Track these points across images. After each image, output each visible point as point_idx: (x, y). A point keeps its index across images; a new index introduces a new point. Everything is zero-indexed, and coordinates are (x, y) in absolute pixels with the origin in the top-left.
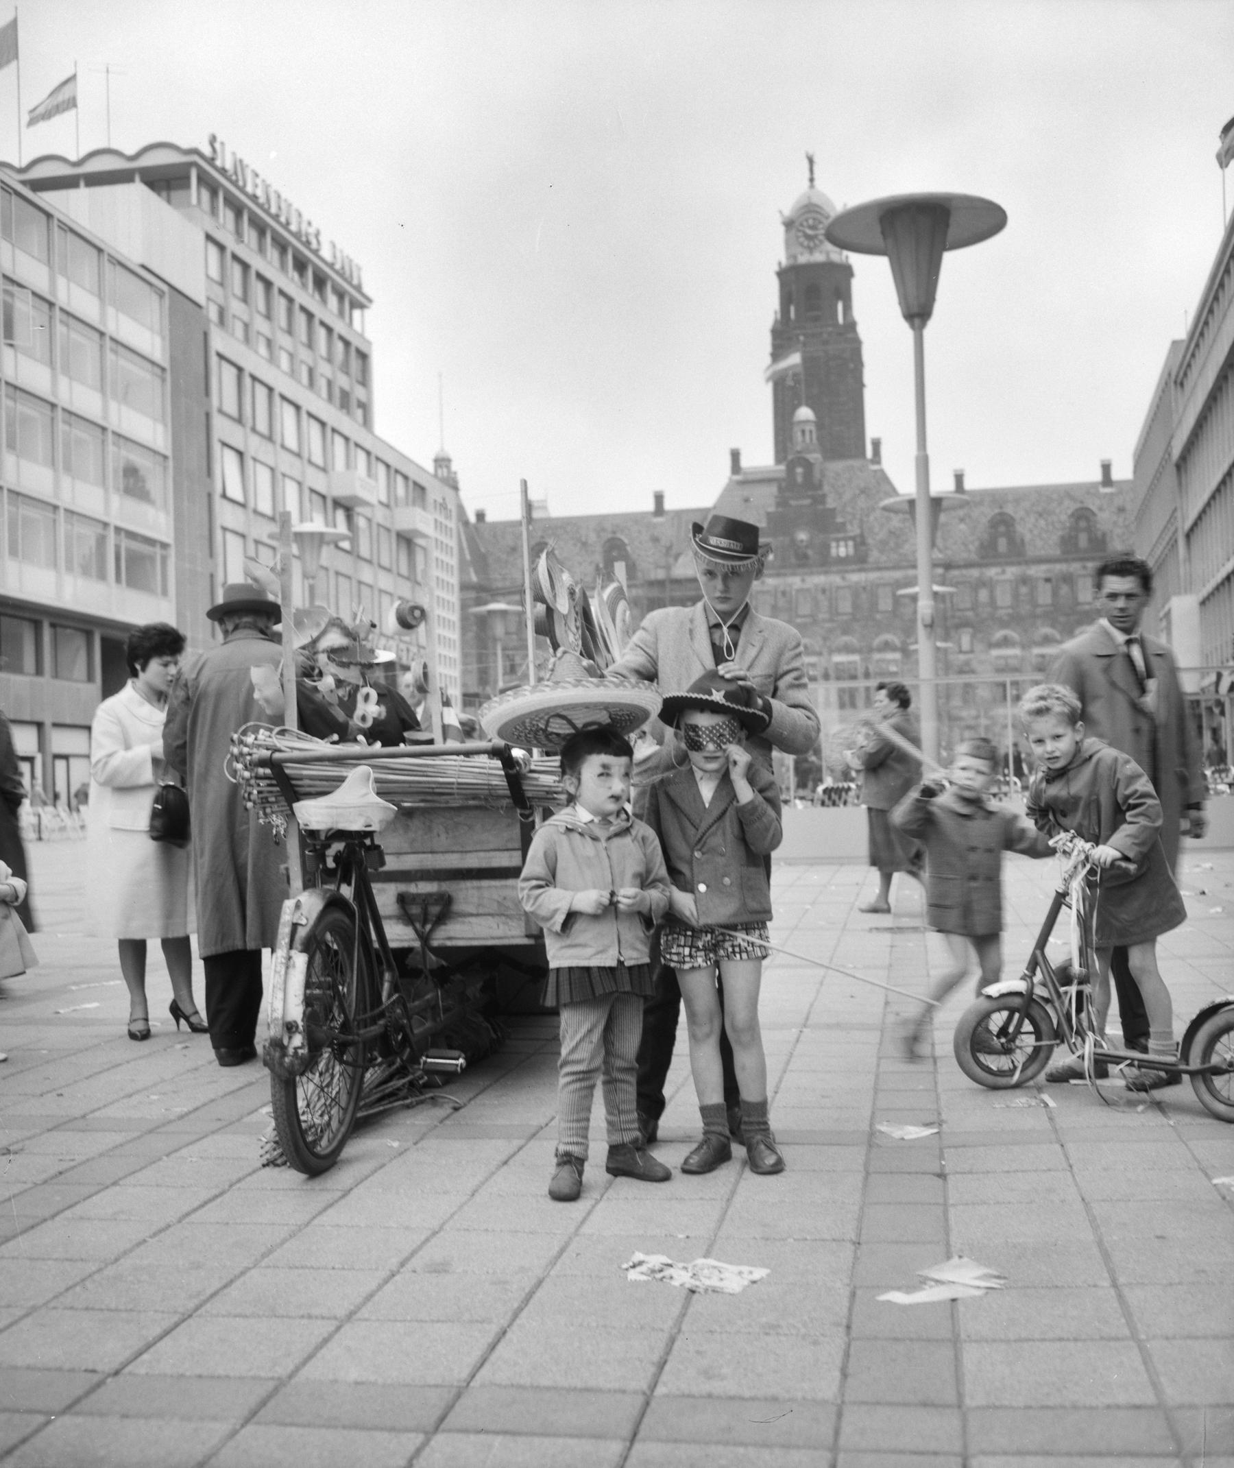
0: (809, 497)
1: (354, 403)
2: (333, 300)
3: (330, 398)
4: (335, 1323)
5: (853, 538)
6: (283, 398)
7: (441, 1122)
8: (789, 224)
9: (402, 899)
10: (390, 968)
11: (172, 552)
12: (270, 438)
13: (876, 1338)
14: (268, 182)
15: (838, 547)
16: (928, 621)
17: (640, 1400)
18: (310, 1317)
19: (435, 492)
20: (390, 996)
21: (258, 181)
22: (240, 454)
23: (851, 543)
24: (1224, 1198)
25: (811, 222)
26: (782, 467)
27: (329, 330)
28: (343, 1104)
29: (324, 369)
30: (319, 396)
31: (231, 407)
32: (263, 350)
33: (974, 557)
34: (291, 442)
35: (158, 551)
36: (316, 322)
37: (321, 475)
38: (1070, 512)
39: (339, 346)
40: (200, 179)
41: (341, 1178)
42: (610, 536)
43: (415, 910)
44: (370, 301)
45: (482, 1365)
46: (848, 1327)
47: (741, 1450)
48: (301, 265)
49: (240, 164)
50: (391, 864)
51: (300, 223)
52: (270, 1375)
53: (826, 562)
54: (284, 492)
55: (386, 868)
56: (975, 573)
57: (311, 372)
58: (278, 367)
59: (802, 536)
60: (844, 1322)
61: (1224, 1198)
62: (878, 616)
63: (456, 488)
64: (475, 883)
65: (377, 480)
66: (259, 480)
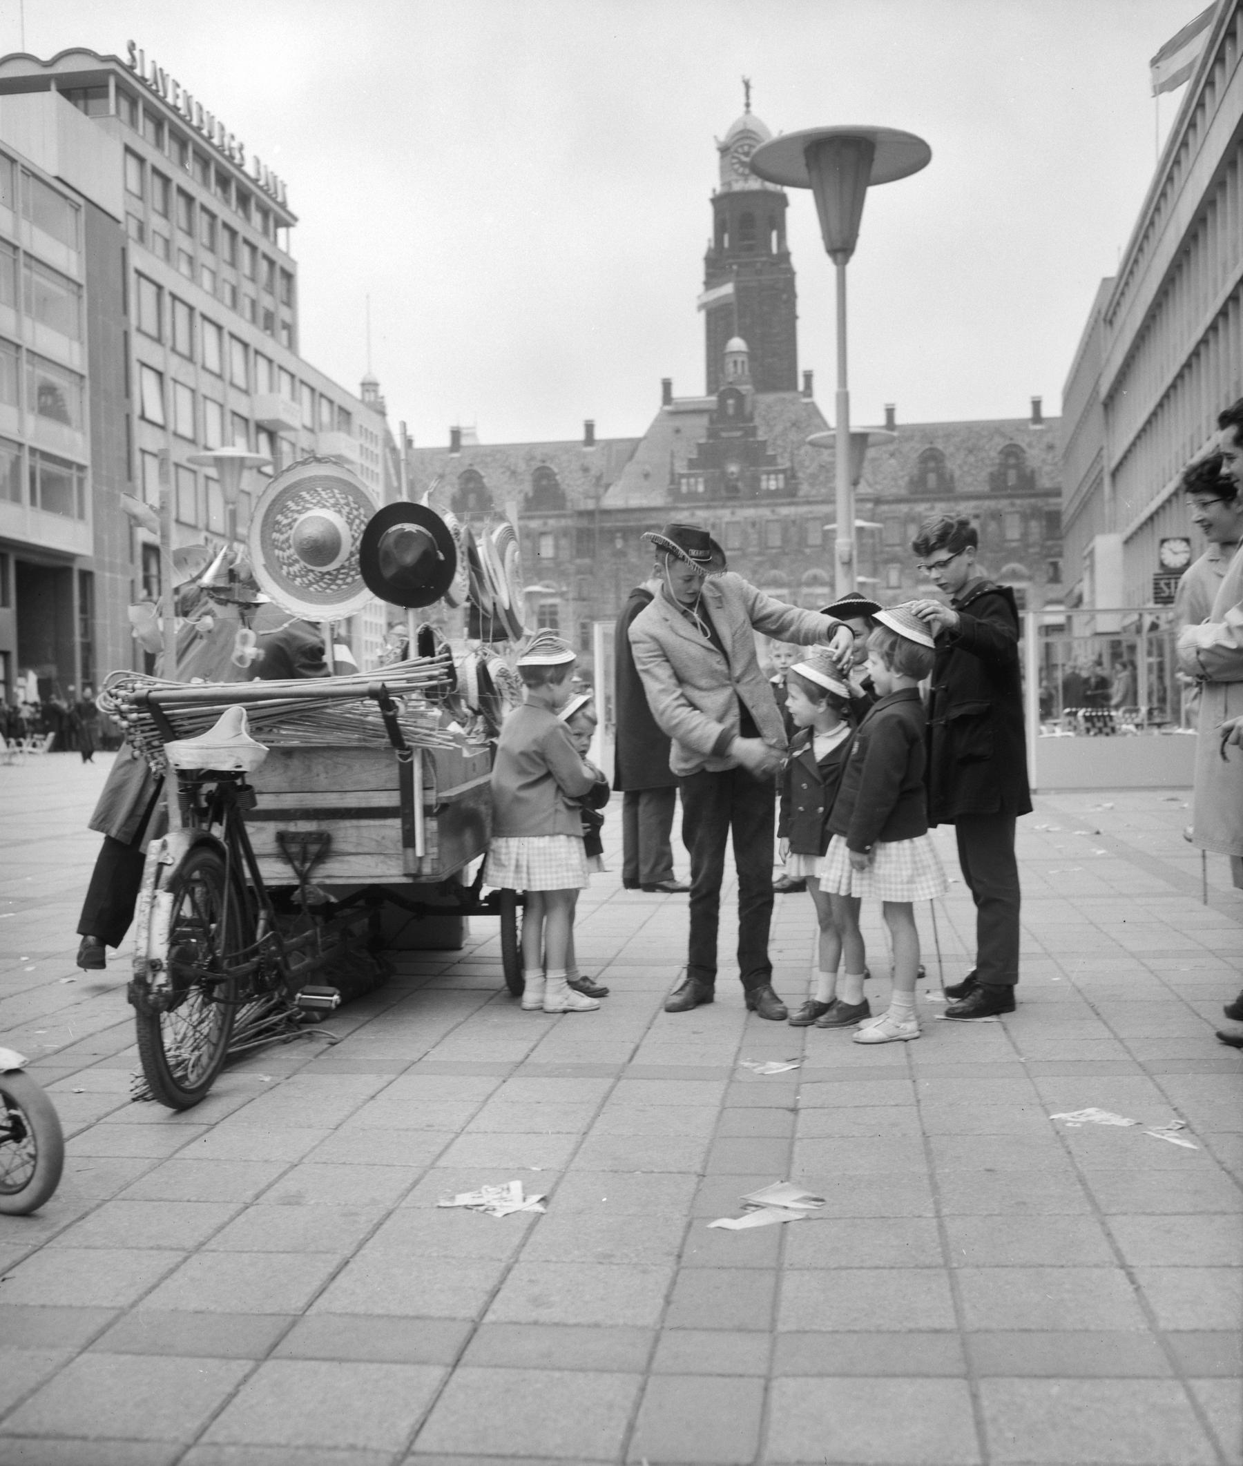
0: (740, 429)
1: (278, 325)
2: (257, 218)
3: (254, 320)
4: (184, 1254)
5: (784, 471)
6: (204, 317)
7: (317, 1056)
8: (724, 150)
9: (281, 838)
10: (265, 907)
11: (89, 474)
12: (190, 359)
13: (703, 1267)
14: (189, 93)
15: (768, 479)
16: (846, 559)
17: (468, 1327)
18: (159, 1248)
19: (362, 417)
20: (265, 932)
21: (179, 91)
22: (160, 375)
23: (781, 476)
24: (1058, 1133)
25: (746, 148)
26: (714, 398)
27: (254, 248)
28: (214, 1040)
29: (248, 288)
30: (242, 316)
31: (150, 326)
32: (184, 268)
33: (903, 492)
34: (213, 363)
35: (74, 472)
36: (240, 239)
37: (244, 398)
38: (999, 448)
39: (264, 265)
40: (118, 88)
41: (207, 1112)
42: (540, 464)
43: (294, 849)
44: (296, 219)
45: (320, 1294)
46: (679, 1256)
47: (557, 1374)
48: (224, 181)
49: (160, 74)
50: (264, 802)
51: (222, 137)
52: (113, 1304)
53: (755, 495)
54: (205, 418)
55: (258, 807)
56: (904, 508)
57: (234, 291)
58: (201, 286)
59: (733, 468)
60: (676, 1251)
61: (1058, 1133)
62: (808, 551)
63: (383, 413)
64: (355, 822)
65: (301, 404)
66: (179, 400)
